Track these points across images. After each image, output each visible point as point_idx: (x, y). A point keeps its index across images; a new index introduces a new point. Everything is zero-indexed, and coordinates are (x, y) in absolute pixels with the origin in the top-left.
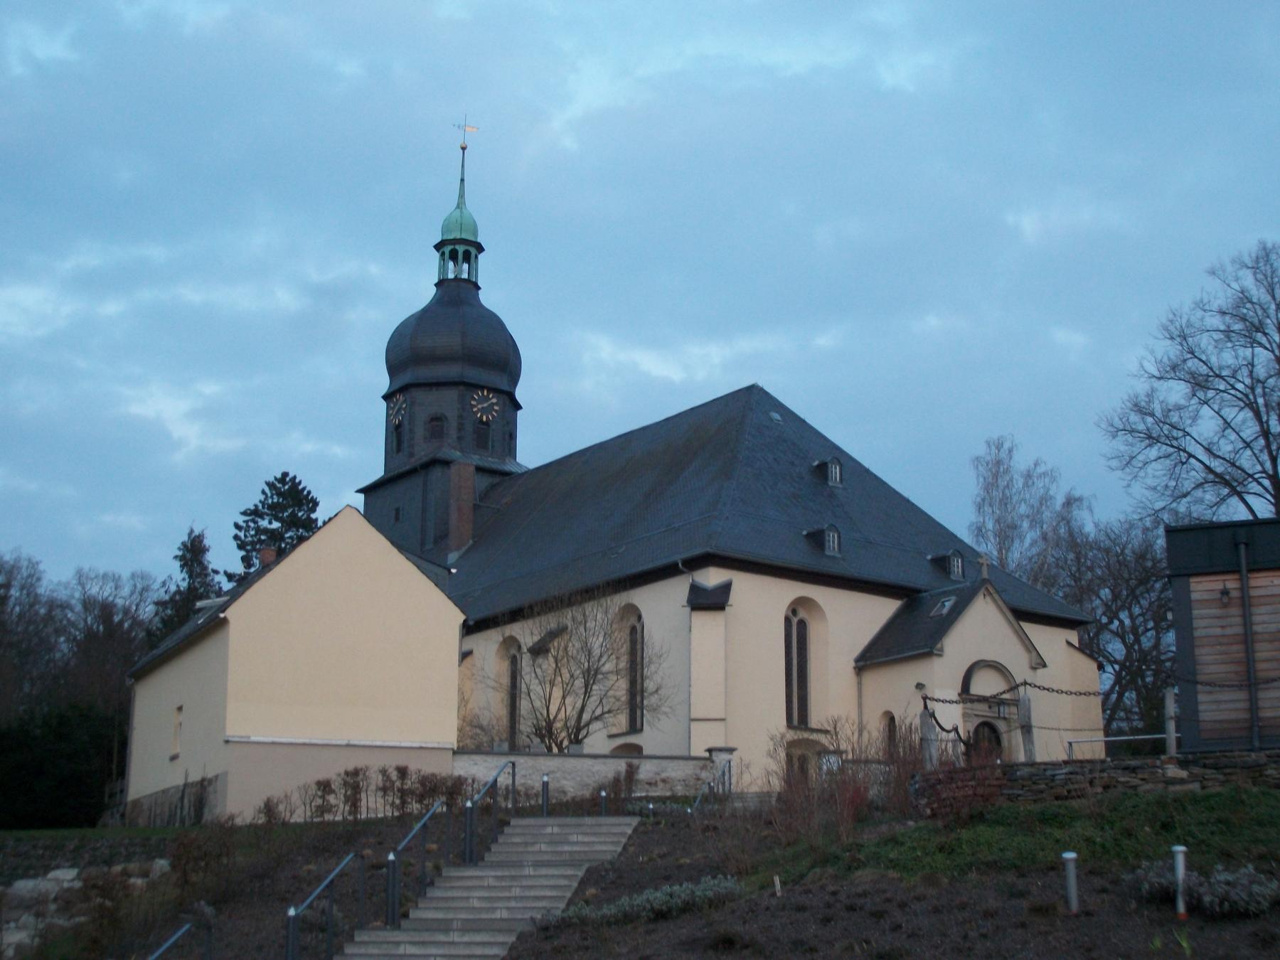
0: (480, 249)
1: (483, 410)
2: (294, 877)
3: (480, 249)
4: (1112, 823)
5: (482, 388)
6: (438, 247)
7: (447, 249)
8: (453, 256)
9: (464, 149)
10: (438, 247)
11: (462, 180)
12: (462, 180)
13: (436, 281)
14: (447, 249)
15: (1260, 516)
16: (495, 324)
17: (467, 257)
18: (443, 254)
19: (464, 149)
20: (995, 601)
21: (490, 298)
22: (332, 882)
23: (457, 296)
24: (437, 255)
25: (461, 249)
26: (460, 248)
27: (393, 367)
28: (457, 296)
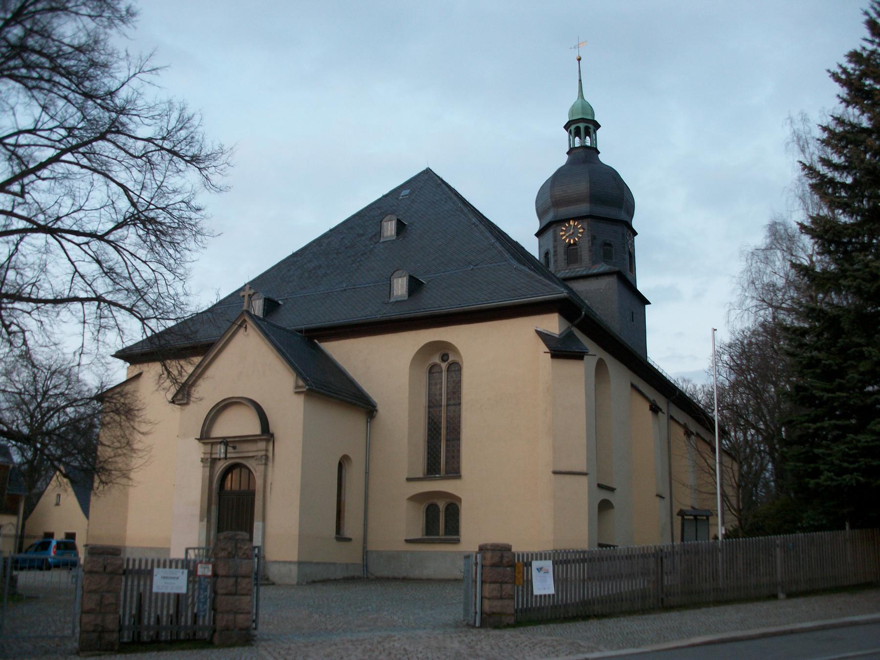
0: (597, 126)
1: (569, 237)
2: (493, 649)
3: (597, 126)
4: (379, 643)
5: (568, 220)
6: (567, 127)
7: (573, 128)
8: (577, 133)
9: (579, 60)
10: (567, 127)
11: (580, 80)
12: (580, 80)
13: (567, 150)
14: (573, 128)
15: (157, 332)
16: (613, 176)
17: (587, 133)
18: (570, 133)
19: (579, 60)
20: (16, 543)
21: (605, 158)
22: (715, 452)
23: (584, 157)
24: (566, 133)
25: (582, 126)
26: (583, 125)
27: (541, 214)
28: (584, 157)
